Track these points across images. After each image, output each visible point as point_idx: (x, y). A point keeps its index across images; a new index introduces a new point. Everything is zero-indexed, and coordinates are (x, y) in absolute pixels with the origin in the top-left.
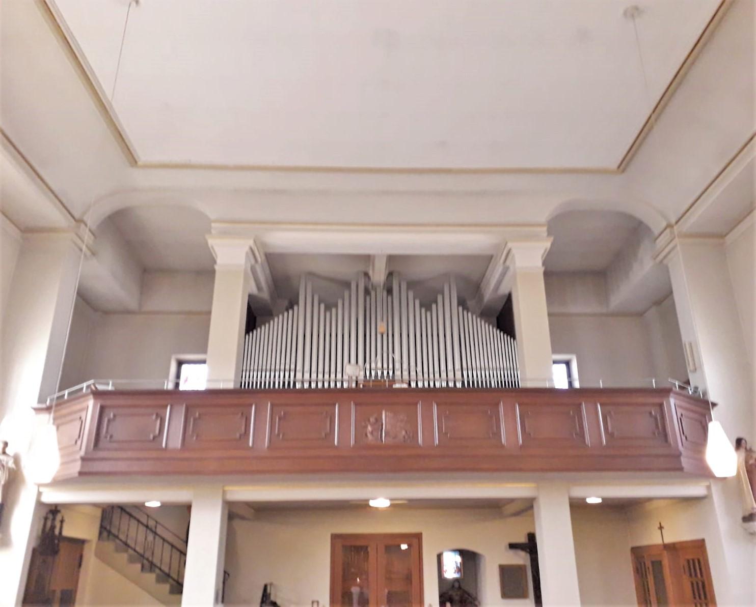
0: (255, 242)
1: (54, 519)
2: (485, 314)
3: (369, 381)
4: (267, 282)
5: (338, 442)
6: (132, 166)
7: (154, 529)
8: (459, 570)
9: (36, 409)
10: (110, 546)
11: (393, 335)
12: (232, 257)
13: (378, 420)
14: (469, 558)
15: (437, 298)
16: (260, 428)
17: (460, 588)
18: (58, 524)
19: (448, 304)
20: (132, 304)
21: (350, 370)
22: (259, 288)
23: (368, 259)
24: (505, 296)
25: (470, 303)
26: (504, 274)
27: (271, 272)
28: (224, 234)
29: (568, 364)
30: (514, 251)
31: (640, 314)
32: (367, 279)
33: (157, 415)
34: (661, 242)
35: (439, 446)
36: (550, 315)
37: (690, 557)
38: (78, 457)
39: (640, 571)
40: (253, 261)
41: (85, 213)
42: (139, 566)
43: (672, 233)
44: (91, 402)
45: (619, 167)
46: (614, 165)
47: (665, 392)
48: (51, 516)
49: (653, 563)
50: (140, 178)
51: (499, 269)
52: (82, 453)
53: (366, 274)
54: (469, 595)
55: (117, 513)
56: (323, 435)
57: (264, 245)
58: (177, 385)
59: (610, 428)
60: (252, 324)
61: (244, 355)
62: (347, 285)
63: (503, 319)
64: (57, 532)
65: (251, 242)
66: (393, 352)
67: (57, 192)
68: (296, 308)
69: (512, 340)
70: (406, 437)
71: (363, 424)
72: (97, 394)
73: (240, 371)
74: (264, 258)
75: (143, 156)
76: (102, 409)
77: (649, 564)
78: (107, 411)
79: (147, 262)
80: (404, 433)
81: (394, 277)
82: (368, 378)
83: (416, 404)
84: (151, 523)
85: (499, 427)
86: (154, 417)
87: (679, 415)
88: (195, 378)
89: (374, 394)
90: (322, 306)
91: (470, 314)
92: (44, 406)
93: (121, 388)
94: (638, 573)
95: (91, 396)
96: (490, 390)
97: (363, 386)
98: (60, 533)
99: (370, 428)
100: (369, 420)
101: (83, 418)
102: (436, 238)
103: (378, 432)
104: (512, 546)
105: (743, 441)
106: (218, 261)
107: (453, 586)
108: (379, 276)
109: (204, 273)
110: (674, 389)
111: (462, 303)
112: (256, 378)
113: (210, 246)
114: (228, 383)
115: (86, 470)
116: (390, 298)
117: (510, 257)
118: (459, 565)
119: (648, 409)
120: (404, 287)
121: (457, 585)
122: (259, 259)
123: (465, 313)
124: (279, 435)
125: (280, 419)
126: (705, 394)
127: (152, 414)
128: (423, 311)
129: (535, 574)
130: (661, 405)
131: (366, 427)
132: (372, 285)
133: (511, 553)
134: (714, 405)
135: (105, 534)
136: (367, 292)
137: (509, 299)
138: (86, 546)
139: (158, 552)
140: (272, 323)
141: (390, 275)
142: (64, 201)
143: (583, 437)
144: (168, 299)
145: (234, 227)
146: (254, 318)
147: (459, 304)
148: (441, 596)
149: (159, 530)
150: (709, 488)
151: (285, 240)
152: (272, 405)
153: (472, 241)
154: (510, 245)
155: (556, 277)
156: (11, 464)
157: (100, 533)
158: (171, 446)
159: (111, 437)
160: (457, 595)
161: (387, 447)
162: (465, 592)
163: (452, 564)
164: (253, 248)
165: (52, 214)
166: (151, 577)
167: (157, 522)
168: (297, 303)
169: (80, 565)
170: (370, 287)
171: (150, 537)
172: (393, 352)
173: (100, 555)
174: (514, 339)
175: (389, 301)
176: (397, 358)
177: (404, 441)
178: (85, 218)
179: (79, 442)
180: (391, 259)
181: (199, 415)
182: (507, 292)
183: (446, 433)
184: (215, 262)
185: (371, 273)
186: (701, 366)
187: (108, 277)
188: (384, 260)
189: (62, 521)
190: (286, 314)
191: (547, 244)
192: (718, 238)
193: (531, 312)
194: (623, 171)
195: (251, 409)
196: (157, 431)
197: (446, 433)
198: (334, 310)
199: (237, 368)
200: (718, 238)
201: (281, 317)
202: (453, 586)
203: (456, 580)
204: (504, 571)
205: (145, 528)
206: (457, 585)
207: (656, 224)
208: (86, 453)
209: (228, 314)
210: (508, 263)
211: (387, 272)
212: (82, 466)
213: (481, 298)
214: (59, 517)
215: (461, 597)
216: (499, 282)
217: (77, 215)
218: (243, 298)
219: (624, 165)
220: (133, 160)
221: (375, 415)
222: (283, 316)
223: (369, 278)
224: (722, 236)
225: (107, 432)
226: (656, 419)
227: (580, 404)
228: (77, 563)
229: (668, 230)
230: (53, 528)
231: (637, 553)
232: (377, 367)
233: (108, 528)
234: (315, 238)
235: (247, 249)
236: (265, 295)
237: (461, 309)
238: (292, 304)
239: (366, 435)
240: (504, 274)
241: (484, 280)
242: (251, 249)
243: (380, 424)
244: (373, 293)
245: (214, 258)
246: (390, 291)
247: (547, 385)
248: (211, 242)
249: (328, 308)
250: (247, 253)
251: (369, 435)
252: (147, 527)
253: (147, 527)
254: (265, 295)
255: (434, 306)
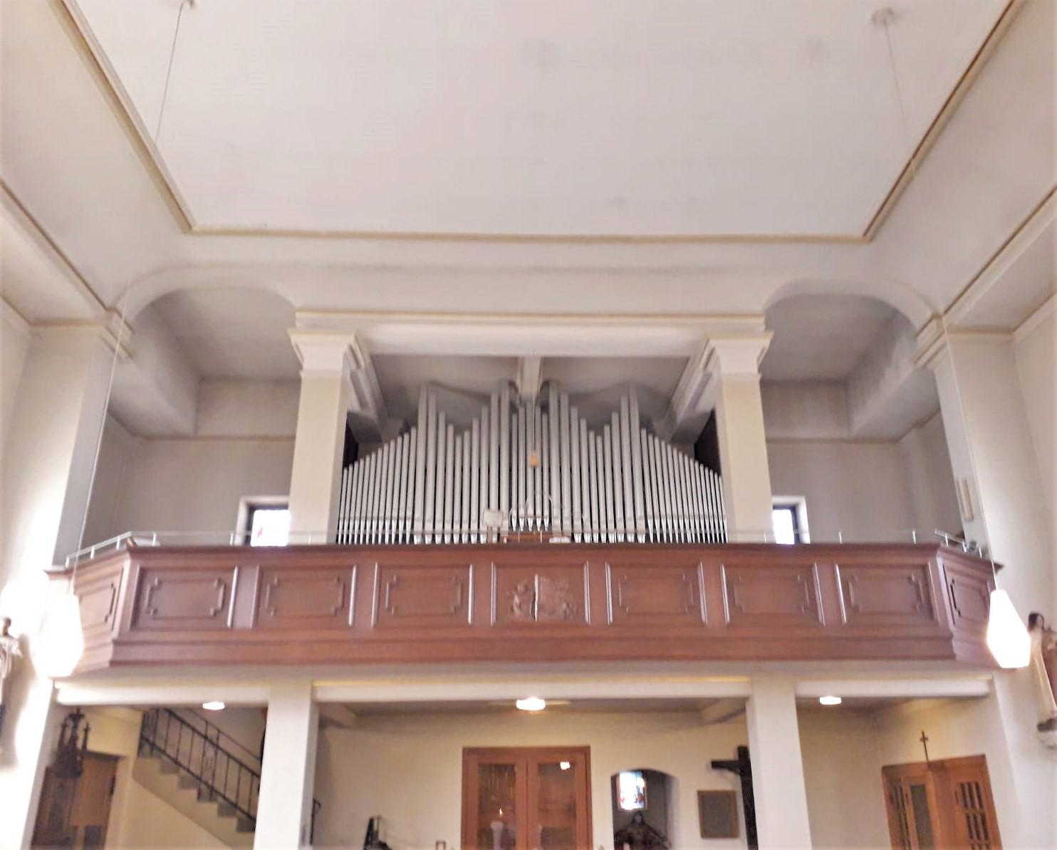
0: (356, 338)
1: (75, 727)
2: (677, 440)
3: (516, 534)
4: (373, 395)
5: (473, 619)
6: (185, 233)
7: (215, 741)
8: (641, 798)
9: (50, 573)
10: (153, 764)
11: (549, 470)
12: (325, 360)
13: (529, 588)
14: (656, 782)
15: (611, 417)
16: (364, 600)
17: (643, 823)
18: (81, 734)
19: (627, 425)
20: (185, 425)
21: (489, 518)
22: (362, 403)
23: (514, 362)
24: (706, 414)
25: (657, 425)
26: (704, 384)
27: (379, 381)
28: (314, 327)
29: (794, 509)
30: (718, 352)
31: (895, 440)
32: (513, 391)
33: (220, 581)
34: (925, 338)
35: (613, 625)
36: (769, 441)
37: (965, 780)
38: (109, 639)
39: (895, 800)
40: (354, 366)
41: (118, 298)
42: (194, 793)
43: (939, 326)
44: (127, 564)
45: (865, 234)
46: (857, 229)
47: (930, 549)
48: (71, 723)
49: (913, 788)
50: (196, 250)
51: (698, 377)
52: (115, 634)
53: (512, 384)
54: (655, 833)
55: (164, 718)
56: (452, 609)
57: (369, 343)
58: (248, 539)
59: (852, 600)
60: (352, 454)
61: (342, 497)
62: (485, 399)
63: (704, 447)
64: (79, 744)
65: (351, 339)
66: (550, 493)
67: (79, 269)
68: (413, 431)
69: (716, 476)
70: (568, 612)
71: (508, 593)
72: (136, 552)
73: (336, 519)
74: (368, 361)
75: (200, 219)
76: (143, 572)
77: (907, 790)
78: (149, 575)
79: (205, 367)
80: (564, 606)
81: (551, 388)
82: (514, 529)
83: (582, 566)
84: (212, 733)
85: (697, 598)
86: (215, 584)
87: (950, 581)
88: (273, 530)
89: (523, 551)
90: (451, 429)
91: (657, 440)
92: (61, 568)
93: (169, 543)
94: (892, 802)
95: (128, 555)
96: (685, 546)
97: (508, 540)
98: (84, 746)
99: (517, 600)
100: (516, 589)
101: (117, 586)
102: (610, 333)
103: (528, 606)
104: (716, 765)
105: (1039, 618)
106: (305, 366)
107: (634, 821)
108: (530, 386)
109: (286, 382)
110: (942, 544)
111: (646, 424)
112: (358, 529)
113: (293, 344)
114: (319, 536)
115: (120, 658)
116: (545, 417)
117: (713, 360)
118: (641, 791)
119: (905, 572)
120: (565, 401)
121: (638, 819)
122: (362, 363)
123: (650, 438)
124: (389, 609)
125: (391, 587)
126: (985, 551)
127: (213, 580)
128: (592, 435)
129: (748, 804)
130: (924, 568)
131: (512, 598)
132: (520, 399)
133: (715, 774)
134: (998, 567)
135: (147, 748)
136: (513, 409)
137: (711, 419)
138: (121, 765)
139: (220, 773)
140: (380, 452)
141: (546, 384)
142: (90, 281)
143: (815, 612)
144: (235, 418)
145: (327, 318)
146: (356, 446)
147: (642, 426)
148: (617, 835)
149: (223, 743)
150: (991, 683)
151: (399, 336)
152: (380, 568)
153: (661, 338)
154: (713, 343)
155: (777, 388)
156: (15, 650)
157: (140, 747)
158: (239, 624)
159: (155, 611)
160: (639, 833)
161: (541, 626)
162: (650, 829)
163: (631, 790)
164: (354, 348)
165: (72, 300)
166: (211, 808)
167: (219, 731)
168: (416, 425)
169: (112, 792)
170: (517, 402)
171: (210, 752)
172: (550, 493)
173: (140, 777)
174: (719, 474)
175: (543, 421)
176: (555, 501)
177: (565, 618)
178: (119, 306)
179: (110, 620)
180: (547, 362)
181: (279, 581)
182: (708, 409)
183: (624, 607)
184: (300, 367)
185: (518, 382)
186: (980, 513)
187: (151, 389)
188: (537, 365)
189: (87, 730)
190: (399, 440)
191: (765, 342)
192: (1004, 333)
193: (743, 437)
194: (872, 239)
195: (351, 573)
196: (220, 604)
197: (624, 607)
198: (467, 435)
199: (331, 515)
200: (1004, 333)
201: (392, 443)
202: (634, 821)
203: (638, 812)
204: (705, 799)
205: (203, 740)
206: (638, 819)
207: (918, 314)
208: (120, 634)
209: (318, 440)
210: (710, 368)
211: (541, 381)
212: (115, 653)
213: (672, 417)
214: (82, 725)
215: (645, 836)
216: (698, 395)
217: (107, 301)
218: (339, 417)
219: (873, 231)
220: (185, 225)
221: (525, 582)
222: (396, 442)
223: (516, 389)
224: (1010, 330)
225: (149, 605)
226: (917, 586)
227: (811, 566)
228: (107, 788)
229: (934, 323)
230: (74, 739)
231: (891, 774)
232: (527, 514)
233: (151, 739)
234: (440, 334)
235: (345, 348)
236: (371, 413)
237: (644, 432)
238: (408, 425)
239: (512, 609)
240: (704, 384)
241: (677, 392)
242: (351, 348)
243: (532, 593)
244: (521, 411)
245: (299, 361)
246: (545, 408)
247: (765, 539)
248: (295, 338)
249: (459, 431)
250: (345, 355)
251: (516, 609)
252: (205, 737)
253: (205, 737)
254: (371, 413)
255: (607, 429)
